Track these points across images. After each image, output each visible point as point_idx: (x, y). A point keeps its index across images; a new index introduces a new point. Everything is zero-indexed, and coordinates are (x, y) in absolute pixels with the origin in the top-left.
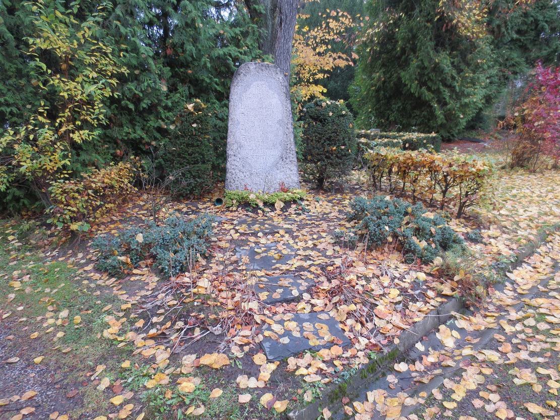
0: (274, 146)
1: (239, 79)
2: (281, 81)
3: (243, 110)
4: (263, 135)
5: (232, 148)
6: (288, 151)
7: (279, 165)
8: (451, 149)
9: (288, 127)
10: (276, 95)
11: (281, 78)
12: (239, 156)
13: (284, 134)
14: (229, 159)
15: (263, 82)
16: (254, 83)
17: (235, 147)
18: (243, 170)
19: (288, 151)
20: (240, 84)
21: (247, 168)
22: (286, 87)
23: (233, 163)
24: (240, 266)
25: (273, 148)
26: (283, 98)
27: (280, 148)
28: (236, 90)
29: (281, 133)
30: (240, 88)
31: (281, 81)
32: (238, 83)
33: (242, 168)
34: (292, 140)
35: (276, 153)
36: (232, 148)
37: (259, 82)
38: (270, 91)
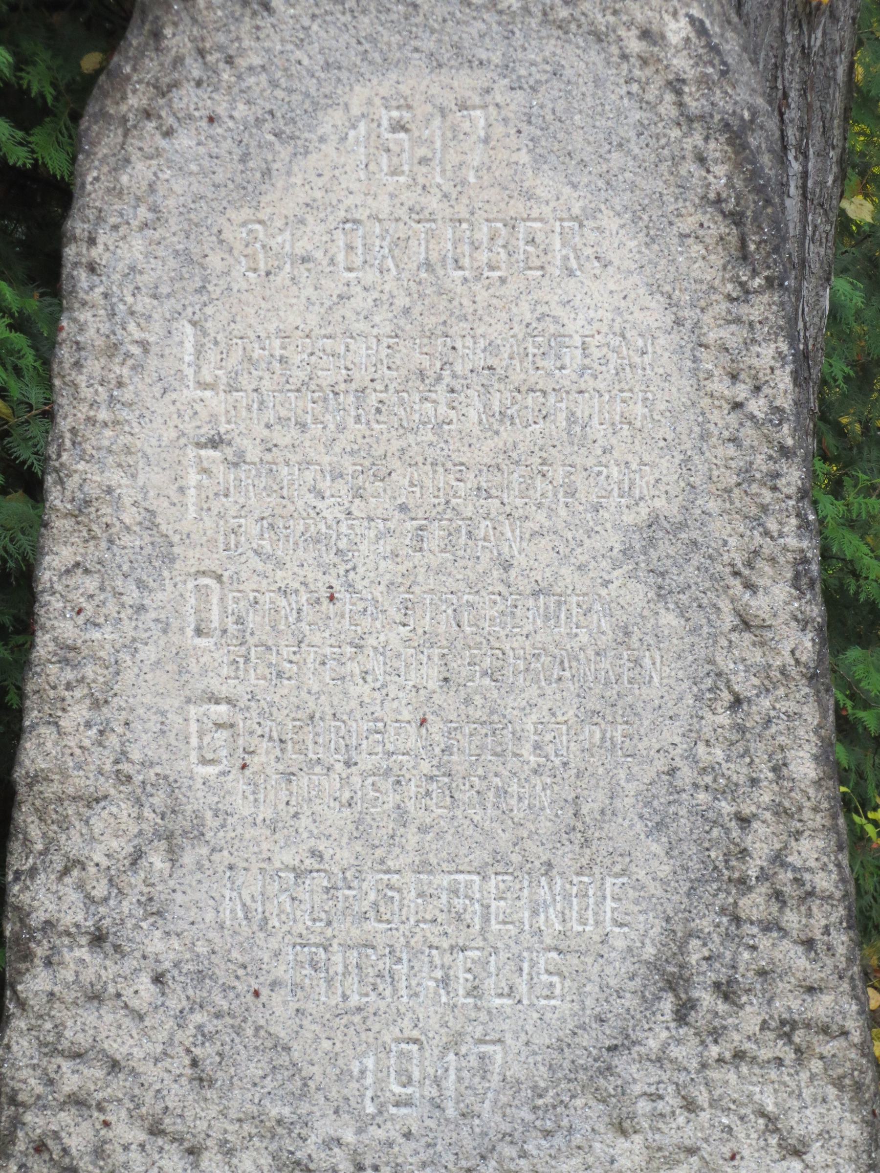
0: (579, 830)
1: (177, 39)
2: (681, 63)
3: (215, 401)
4: (449, 701)
5: (73, 843)
6: (755, 904)
7: (638, 1076)
8: (849, 927)
9: (759, 605)
10: (620, 241)
11: (677, 30)
12: (156, 944)
13: (705, 700)
14: (35, 983)
15: (466, 82)
16: (358, 98)
17: (106, 836)
18: (202, 1116)
19: (755, 904)
20: (186, 98)
21: (240, 1100)
22: (736, 135)
23: (81, 1025)
24: (792, 65)
25: (566, 858)
26: (704, 264)
27: (652, 860)
28: (139, 172)
29: (664, 678)
30: (184, 140)
31: (681, 63)
32: (163, 91)
33: (178, 1093)
34: (804, 766)
35: (611, 915)
36: (73, 843)
37: (417, 81)
38: (545, 184)
